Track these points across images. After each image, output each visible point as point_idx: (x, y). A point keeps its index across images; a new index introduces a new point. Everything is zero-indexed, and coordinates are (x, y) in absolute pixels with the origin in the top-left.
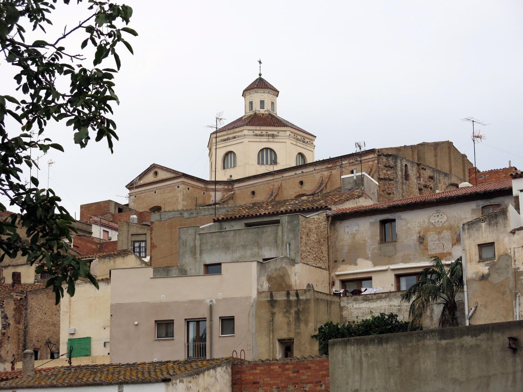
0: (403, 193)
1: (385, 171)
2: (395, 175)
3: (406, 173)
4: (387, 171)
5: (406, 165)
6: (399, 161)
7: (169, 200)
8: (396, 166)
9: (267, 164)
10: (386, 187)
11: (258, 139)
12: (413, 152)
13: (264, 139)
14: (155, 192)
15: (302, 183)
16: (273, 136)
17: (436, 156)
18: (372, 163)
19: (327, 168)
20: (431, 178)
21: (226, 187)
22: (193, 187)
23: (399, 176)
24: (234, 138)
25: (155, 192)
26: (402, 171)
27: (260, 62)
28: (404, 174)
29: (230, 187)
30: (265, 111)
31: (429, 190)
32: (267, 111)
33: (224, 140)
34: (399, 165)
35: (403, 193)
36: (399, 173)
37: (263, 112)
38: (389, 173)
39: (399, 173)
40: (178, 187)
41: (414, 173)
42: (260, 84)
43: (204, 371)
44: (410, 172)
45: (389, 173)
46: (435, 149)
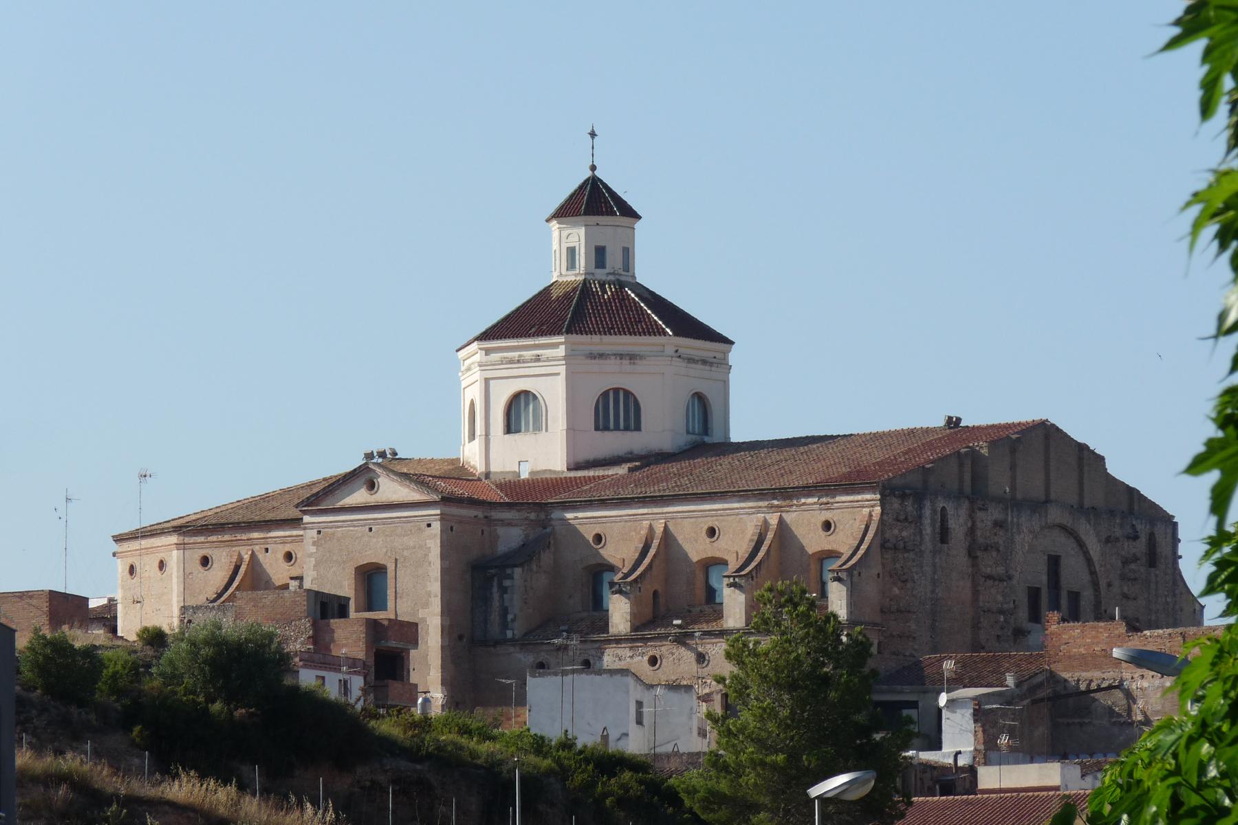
0: (934, 573)
1: (896, 532)
2: (918, 538)
3: (942, 525)
4: (901, 531)
5: (943, 509)
6: (928, 504)
7: (405, 553)
8: (920, 517)
9: (617, 428)
10: (898, 566)
11: (595, 365)
12: (961, 465)
13: (611, 365)
14: (370, 530)
15: (712, 532)
16: (632, 357)
17: (1013, 467)
18: (868, 510)
19: (772, 506)
20: (998, 524)
21: (533, 516)
22: (461, 522)
23: (927, 538)
24: (538, 359)
25: (370, 530)
26: (933, 524)
27: (593, 135)
28: (938, 530)
29: (542, 516)
30: (609, 274)
31: (994, 554)
32: (613, 274)
33: (511, 361)
34: (927, 512)
35: (934, 573)
36: (928, 530)
37: (604, 278)
38: (905, 534)
39: (928, 530)
40: (429, 525)
41: (961, 520)
42: (594, 201)
43: (429, 756)
44: (952, 524)
45: (905, 534)
46: (1013, 451)
